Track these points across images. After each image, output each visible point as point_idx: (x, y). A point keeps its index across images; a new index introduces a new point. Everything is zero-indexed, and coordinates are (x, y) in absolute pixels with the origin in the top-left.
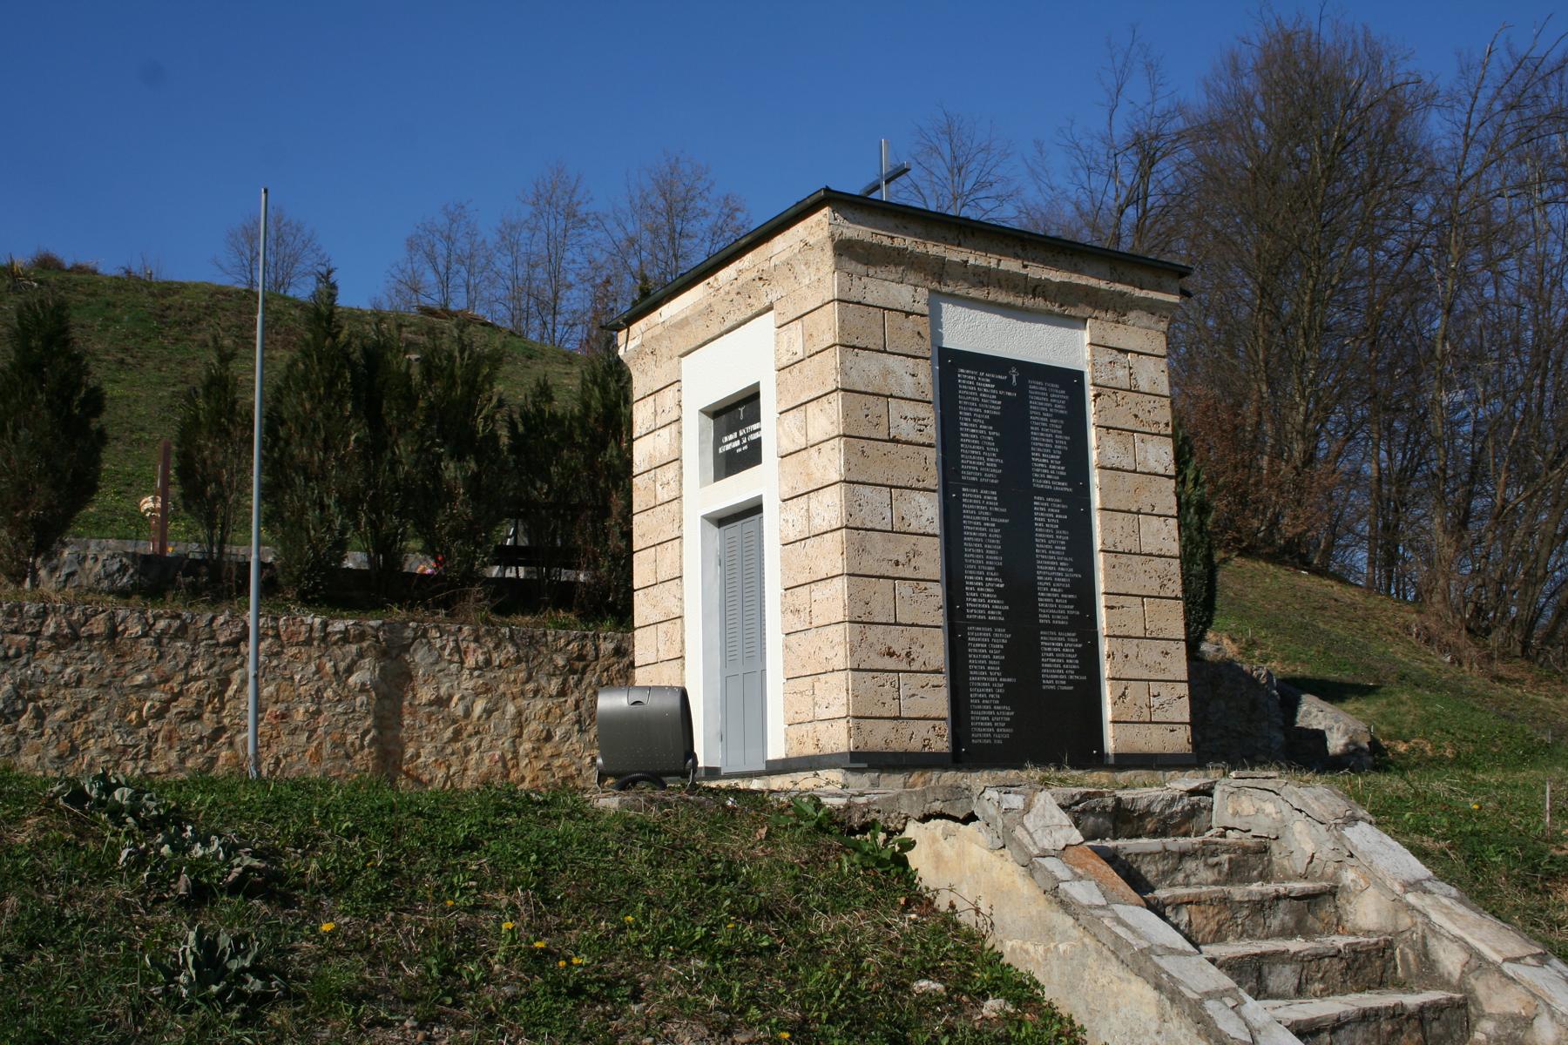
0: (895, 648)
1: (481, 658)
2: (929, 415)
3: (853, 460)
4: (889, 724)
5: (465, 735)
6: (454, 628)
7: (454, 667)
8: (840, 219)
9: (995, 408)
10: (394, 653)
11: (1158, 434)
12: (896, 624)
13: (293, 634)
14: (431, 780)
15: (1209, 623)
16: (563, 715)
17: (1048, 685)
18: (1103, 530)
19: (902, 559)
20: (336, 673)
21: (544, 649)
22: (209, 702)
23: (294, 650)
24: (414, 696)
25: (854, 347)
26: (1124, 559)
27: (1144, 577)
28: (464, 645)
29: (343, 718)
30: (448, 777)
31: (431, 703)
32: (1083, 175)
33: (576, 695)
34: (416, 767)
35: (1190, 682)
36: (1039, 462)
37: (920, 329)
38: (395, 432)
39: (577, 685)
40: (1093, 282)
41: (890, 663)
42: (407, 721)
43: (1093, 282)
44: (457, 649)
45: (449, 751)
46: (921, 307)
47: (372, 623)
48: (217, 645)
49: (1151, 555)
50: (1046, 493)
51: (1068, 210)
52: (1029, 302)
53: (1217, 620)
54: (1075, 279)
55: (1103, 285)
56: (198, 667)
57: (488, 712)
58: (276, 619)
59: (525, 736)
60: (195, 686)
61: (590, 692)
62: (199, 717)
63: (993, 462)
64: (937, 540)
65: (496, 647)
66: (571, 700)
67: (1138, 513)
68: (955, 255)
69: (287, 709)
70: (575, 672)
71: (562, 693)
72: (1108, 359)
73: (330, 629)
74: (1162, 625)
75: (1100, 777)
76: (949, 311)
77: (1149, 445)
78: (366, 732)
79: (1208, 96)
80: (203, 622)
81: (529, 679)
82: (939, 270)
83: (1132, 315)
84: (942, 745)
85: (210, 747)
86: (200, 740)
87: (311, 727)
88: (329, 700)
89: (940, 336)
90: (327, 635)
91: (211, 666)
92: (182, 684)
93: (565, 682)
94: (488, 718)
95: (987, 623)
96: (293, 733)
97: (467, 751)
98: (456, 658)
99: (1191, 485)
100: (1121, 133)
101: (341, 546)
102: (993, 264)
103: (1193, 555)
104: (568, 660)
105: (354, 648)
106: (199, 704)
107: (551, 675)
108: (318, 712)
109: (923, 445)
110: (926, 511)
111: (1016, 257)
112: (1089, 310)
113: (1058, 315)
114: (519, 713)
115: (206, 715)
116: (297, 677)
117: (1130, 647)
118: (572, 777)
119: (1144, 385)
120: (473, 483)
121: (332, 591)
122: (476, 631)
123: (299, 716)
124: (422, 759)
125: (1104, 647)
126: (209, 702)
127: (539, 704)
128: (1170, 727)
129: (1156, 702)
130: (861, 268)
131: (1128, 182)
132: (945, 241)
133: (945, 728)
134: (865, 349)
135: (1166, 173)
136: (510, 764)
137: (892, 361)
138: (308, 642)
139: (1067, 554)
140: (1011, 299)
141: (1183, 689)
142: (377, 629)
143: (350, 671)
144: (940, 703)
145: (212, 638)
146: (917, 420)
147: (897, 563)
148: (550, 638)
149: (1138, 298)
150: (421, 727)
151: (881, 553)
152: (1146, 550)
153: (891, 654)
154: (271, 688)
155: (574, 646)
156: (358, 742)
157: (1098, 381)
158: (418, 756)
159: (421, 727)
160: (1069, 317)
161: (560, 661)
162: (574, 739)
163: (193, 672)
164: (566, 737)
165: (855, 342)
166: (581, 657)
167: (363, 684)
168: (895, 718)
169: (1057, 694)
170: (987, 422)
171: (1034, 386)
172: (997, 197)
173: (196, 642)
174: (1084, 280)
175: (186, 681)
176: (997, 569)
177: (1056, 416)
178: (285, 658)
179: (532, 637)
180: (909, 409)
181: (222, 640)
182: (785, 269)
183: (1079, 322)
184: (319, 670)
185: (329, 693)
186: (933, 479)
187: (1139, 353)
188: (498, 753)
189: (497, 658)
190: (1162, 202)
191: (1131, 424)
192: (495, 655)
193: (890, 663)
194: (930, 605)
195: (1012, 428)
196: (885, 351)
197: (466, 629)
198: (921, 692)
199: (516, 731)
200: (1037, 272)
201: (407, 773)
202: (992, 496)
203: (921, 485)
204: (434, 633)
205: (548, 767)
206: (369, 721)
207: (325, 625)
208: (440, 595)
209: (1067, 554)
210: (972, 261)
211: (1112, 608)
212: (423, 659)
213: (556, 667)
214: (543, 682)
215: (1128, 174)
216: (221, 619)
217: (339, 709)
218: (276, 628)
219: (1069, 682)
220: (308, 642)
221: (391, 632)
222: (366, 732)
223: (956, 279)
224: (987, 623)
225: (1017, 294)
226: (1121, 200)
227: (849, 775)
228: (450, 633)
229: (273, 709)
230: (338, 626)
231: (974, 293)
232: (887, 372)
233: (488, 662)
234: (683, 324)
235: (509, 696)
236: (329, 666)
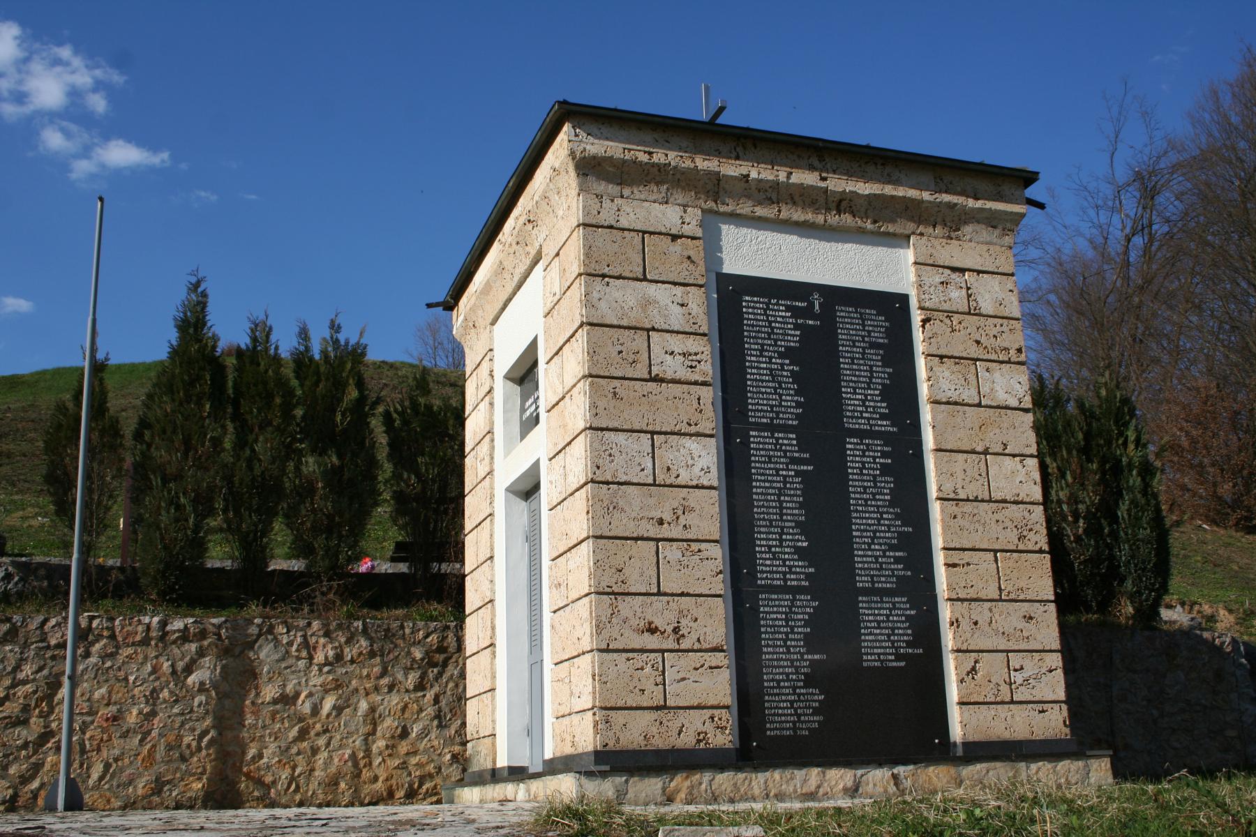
0: (659, 622)
1: (331, 653)
2: (705, 350)
3: (602, 404)
4: (650, 716)
5: (312, 733)
6: (302, 623)
7: (302, 664)
8: (583, 134)
9: (793, 339)
10: (237, 651)
11: (1009, 362)
12: (659, 594)
13: (129, 634)
14: (274, 782)
15: (1164, 589)
16: (421, 710)
17: (870, 661)
18: (940, 473)
19: (667, 516)
20: (174, 672)
21: (400, 642)
22: (37, 706)
23: (130, 651)
24: (258, 694)
25: (604, 276)
26: (968, 507)
27: (994, 529)
28: (313, 640)
29: (180, 719)
30: (292, 779)
31: (275, 702)
32: (1092, 213)
33: (436, 689)
34: (259, 769)
35: (1067, 651)
36: (852, 400)
37: (691, 253)
38: (257, 429)
39: (436, 679)
40: (912, 193)
41: (652, 641)
42: (249, 720)
43: (912, 193)
44: (305, 644)
45: (294, 750)
46: (692, 228)
47: (214, 621)
48: (48, 647)
49: (1004, 501)
50: (861, 434)
51: (1082, 244)
52: (833, 219)
53: (1175, 582)
54: (889, 190)
55: (926, 196)
56: (27, 670)
57: (338, 709)
58: (112, 619)
59: (379, 734)
60: (21, 691)
61: (451, 685)
62: (25, 722)
63: (789, 400)
64: (715, 493)
65: (348, 641)
66: (430, 695)
67: (986, 452)
68: (732, 169)
69: (119, 711)
70: (435, 665)
71: (420, 687)
72: (938, 279)
73: (168, 628)
74: (1022, 584)
75: (936, 775)
76: (730, 233)
77: (997, 375)
78: (204, 733)
79: (1194, 126)
80: (34, 624)
81: (384, 673)
82: (714, 187)
83: (968, 229)
84: (723, 739)
85: (35, 752)
86: (25, 745)
87: (144, 729)
88: (165, 701)
89: (720, 261)
90: (165, 634)
91: (40, 669)
92: (8, 688)
93: (422, 677)
94: (338, 715)
95: (784, 589)
96: (125, 735)
97: (315, 751)
98: (304, 654)
99: (1131, 446)
100: (1122, 175)
101: (198, 546)
102: (782, 177)
103: (1138, 519)
104: (427, 653)
105: (193, 647)
106: (26, 709)
107: (407, 670)
108: (153, 713)
109: (696, 383)
110: (701, 459)
111: (812, 168)
112: (911, 226)
113: (872, 232)
114: (373, 709)
115: (33, 720)
116: (132, 678)
117: (981, 612)
118: (431, 776)
119: (987, 306)
120: (333, 476)
121: (189, 587)
122: (326, 626)
123: (132, 718)
124: (265, 760)
125: (946, 612)
126: (37, 706)
127: (395, 700)
128: (1040, 707)
129: (1018, 678)
130: (613, 189)
131: (1132, 214)
132: (718, 154)
133: (729, 719)
134: (619, 277)
135: (1169, 204)
136: (362, 763)
137: (652, 290)
138: (145, 642)
139: (892, 504)
140: (810, 216)
141: (1056, 660)
142: (220, 627)
143: (189, 670)
144: (719, 686)
145: (42, 641)
146: (688, 355)
147: (661, 522)
148: (407, 631)
149: (973, 209)
150: (264, 727)
151: (637, 510)
152: (997, 495)
153: (652, 630)
154: (103, 690)
155: (433, 638)
156: (194, 744)
157: (927, 305)
158: (261, 756)
159: (264, 727)
160: (887, 234)
161: (418, 654)
162: (433, 736)
163: (21, 676)
164: (425, 733)
165: (606, 271)
166: (441, 649)
167: (202, 683)
168: (657, 708)
169: (884, 671)
170: (781, 355)
171: (844, 313)
172: (1023, 243)
173: (26, 646)
174: (901, 192)
175: (13, 686)
176: (798, 524)
177: (873, 345)
178: (120, 659)
179: (388, 630)
180: (676, 343)
181: (53, 642)
182: (544, 203)
183: (901, 240)
184: (155, 670)
185: (165, 694)
186: (710, 421)
187: (979, 272)
188: (349, 751)
189: (348, 653)
190: (1166, 229)
191: (974, 351)
192: (347, 650)
193: (652, 641)
194: (708, 569)
195: (816, 361)
196: (645, 279)
197: (316, 624)
198: (694, 675)
199: (370, 727)
200: (838, 184)
201: (248, 775)
202: (789, 441)
203: (693, 429)
204: (282, 629)
205: (403, 766)
206: (208, 722)
207: (163, 624)
208: (287, 593)
209: (892, 504)
210: (754, 175)
211: (954, 565)
212: (268, 656)
213: (414, 660)
214: (400, 676)
215: (1130, 204)
216: (53, 622)
217: (175, 710)
218: (112, 629)
219: (899, 657)
220: (145, 642)
221: (234, 629)
222: (204, 733)
223: (737, 197)
224: (784, 589)
225: (817, 211)
226: (1128, 230)
227: (584, 780)
228: (298, 629)
229: (104, 711)
230: (177, 625)
231: (760, 211)
232: (647, 303)
233: (339, 657)
234: (487, 288)
235: (362, 692)
236: (166, 666)
